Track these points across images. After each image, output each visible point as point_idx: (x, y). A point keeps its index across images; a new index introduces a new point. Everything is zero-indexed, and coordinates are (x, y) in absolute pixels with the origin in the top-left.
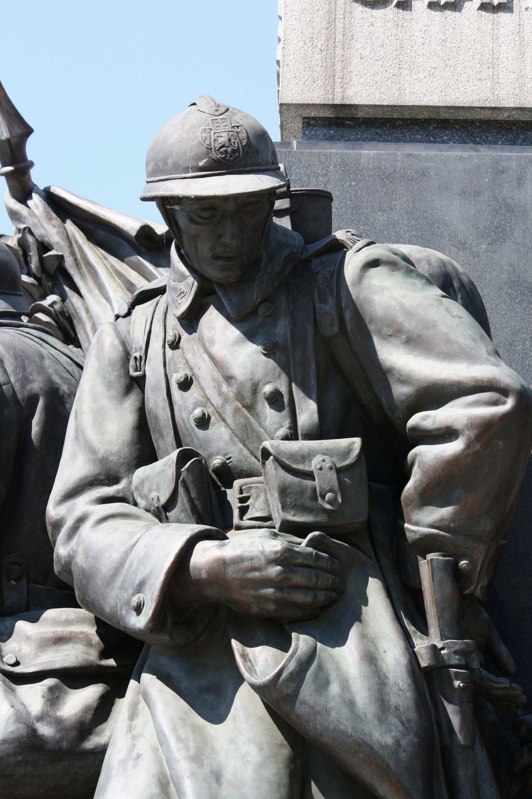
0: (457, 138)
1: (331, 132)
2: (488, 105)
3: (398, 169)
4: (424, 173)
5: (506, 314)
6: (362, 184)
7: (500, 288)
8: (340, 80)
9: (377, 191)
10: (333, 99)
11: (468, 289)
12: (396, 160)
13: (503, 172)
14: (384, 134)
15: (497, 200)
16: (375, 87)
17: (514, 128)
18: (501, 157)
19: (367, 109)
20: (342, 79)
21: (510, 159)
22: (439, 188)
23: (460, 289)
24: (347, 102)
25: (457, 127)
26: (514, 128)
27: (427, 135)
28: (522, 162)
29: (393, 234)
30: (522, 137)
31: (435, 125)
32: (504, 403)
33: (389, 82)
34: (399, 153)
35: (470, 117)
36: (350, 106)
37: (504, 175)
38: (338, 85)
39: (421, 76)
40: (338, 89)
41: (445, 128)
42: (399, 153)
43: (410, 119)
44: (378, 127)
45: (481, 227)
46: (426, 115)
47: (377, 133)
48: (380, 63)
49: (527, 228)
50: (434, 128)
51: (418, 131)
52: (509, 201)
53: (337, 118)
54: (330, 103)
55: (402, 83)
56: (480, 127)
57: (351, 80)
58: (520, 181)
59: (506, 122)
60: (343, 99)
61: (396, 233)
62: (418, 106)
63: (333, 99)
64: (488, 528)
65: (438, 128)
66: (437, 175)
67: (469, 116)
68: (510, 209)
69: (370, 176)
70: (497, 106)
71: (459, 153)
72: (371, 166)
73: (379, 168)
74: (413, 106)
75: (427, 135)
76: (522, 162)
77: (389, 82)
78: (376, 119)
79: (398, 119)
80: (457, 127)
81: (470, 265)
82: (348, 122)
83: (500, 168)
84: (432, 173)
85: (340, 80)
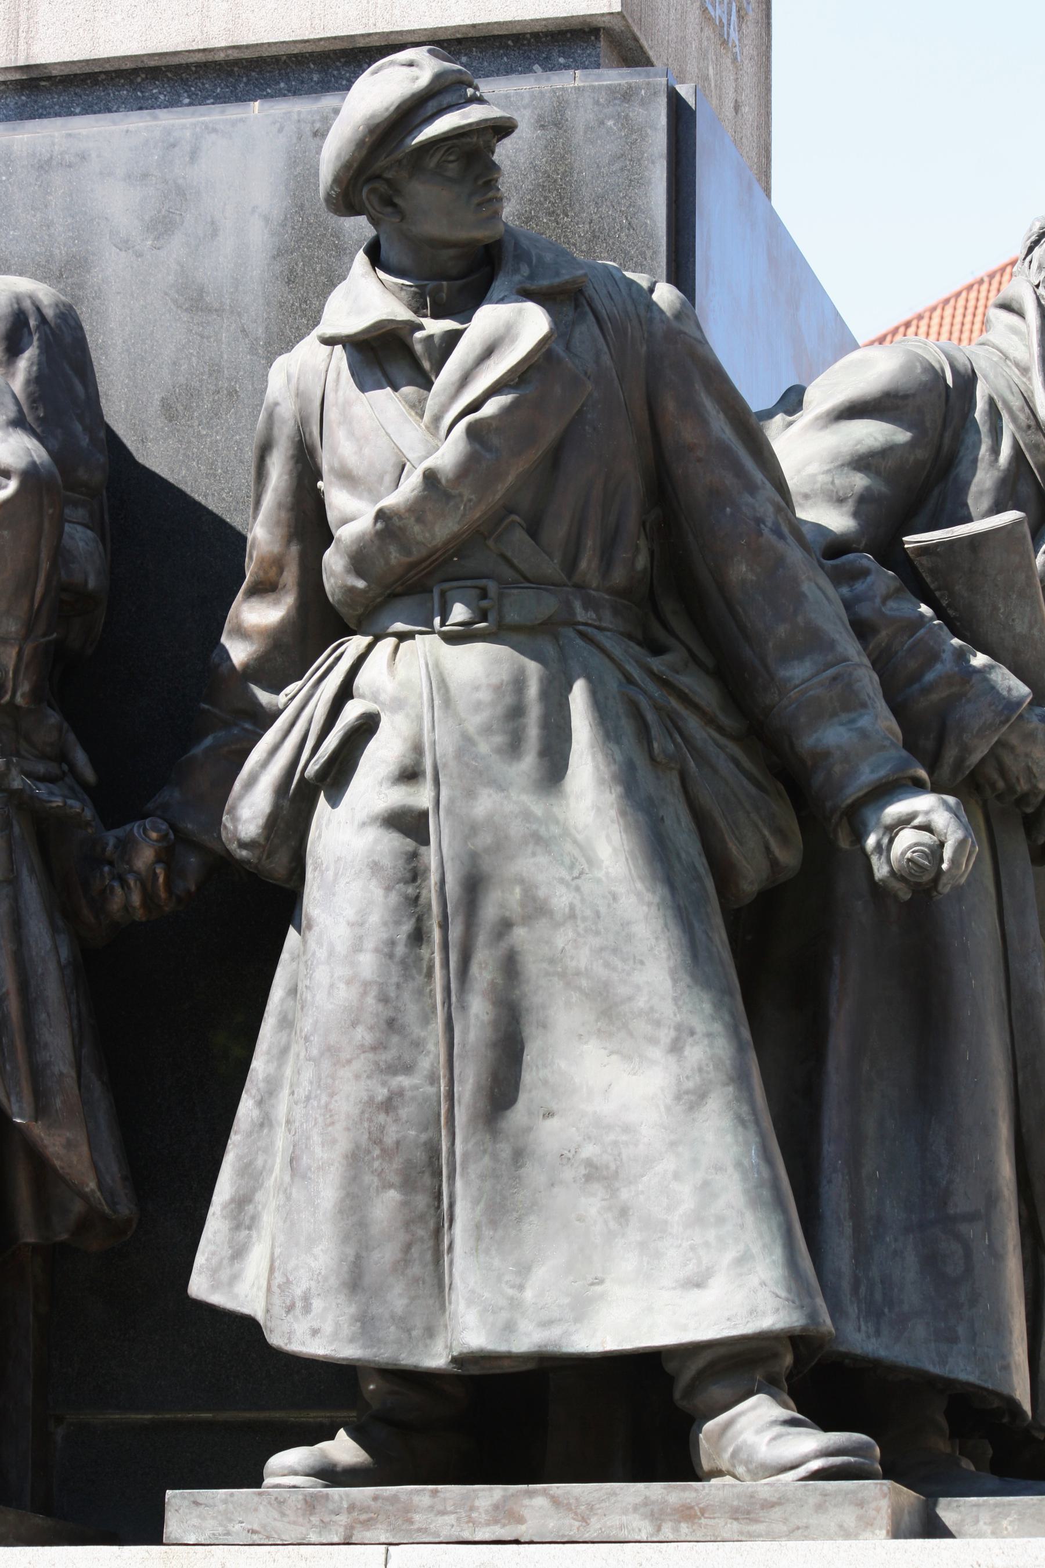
0: (168, 89)
1: (23, 98)
2: (195, 47)
3: (55, 153)
4: (83, 157)
5: (171, 326)
6: (14, 177)
7: (166, 294)
8: (24, 35)
9: (31, 184)
10: (16, 59)
11: (53, 325)
12: (54, 144)
13: (174, 146)
14: (85, 94)
15: (166, 182)
16: (64, 39)
17: (236, 69)
18: (173, 125)
19: (58, 67)
20: (27, 32)
21: (184, 127)
22: (101, 173)
23: (38, 327)
24: (32, 62)
25: (169, 75)
26: (236, 69)
27: (134, 90)
28: (198, 129)
29: (47, 237)
30: (245, 79)
31: (143, 76)
32: (5, 487)
33: (81, 30)
34: (56, 134)
35: (183, 62)
36: (37, 66)
37: (176, 149)
38: (22, 41)
39: (118, 18)
40: (22, 47)
41: (155, 78)
42: (56, 134)
43: (115, 71)
44: (78, 86)
45: (147, 218)
46: (129, 65)
47: (76, 94)
48: (71, 7)
49: (200, 215)
50: (143, 80)
51: (123, 85)
52: (180, 181)
53: (31, 79)
54: (13, 65)
55: (96, 29)
56: (196, 72)
57: (37, 32)
58: (194, 155)
59: (227, 62)
60: (27, 58)
61: (49, 236)
62: (114, 58)
63: (16, 59)
64: (13, 629)
65: (147, 78)
66: (99, 156)
67: (176, 61)
68: (181, 192)
69: (23, 167)
70: (206, 47)
71: (125, 127)
72: (25, 154)
73: (34, 155)
74: (108, 58)
75: (134, 90)
76: (198, 129)
77: (81, 30)
78: (75, 75)
79: (101, 72)
80: (169, 75)
81: (132, 268)
82: (43, 83)
83: (172, 140)
84: (94, 155)
85: (24, 35)
